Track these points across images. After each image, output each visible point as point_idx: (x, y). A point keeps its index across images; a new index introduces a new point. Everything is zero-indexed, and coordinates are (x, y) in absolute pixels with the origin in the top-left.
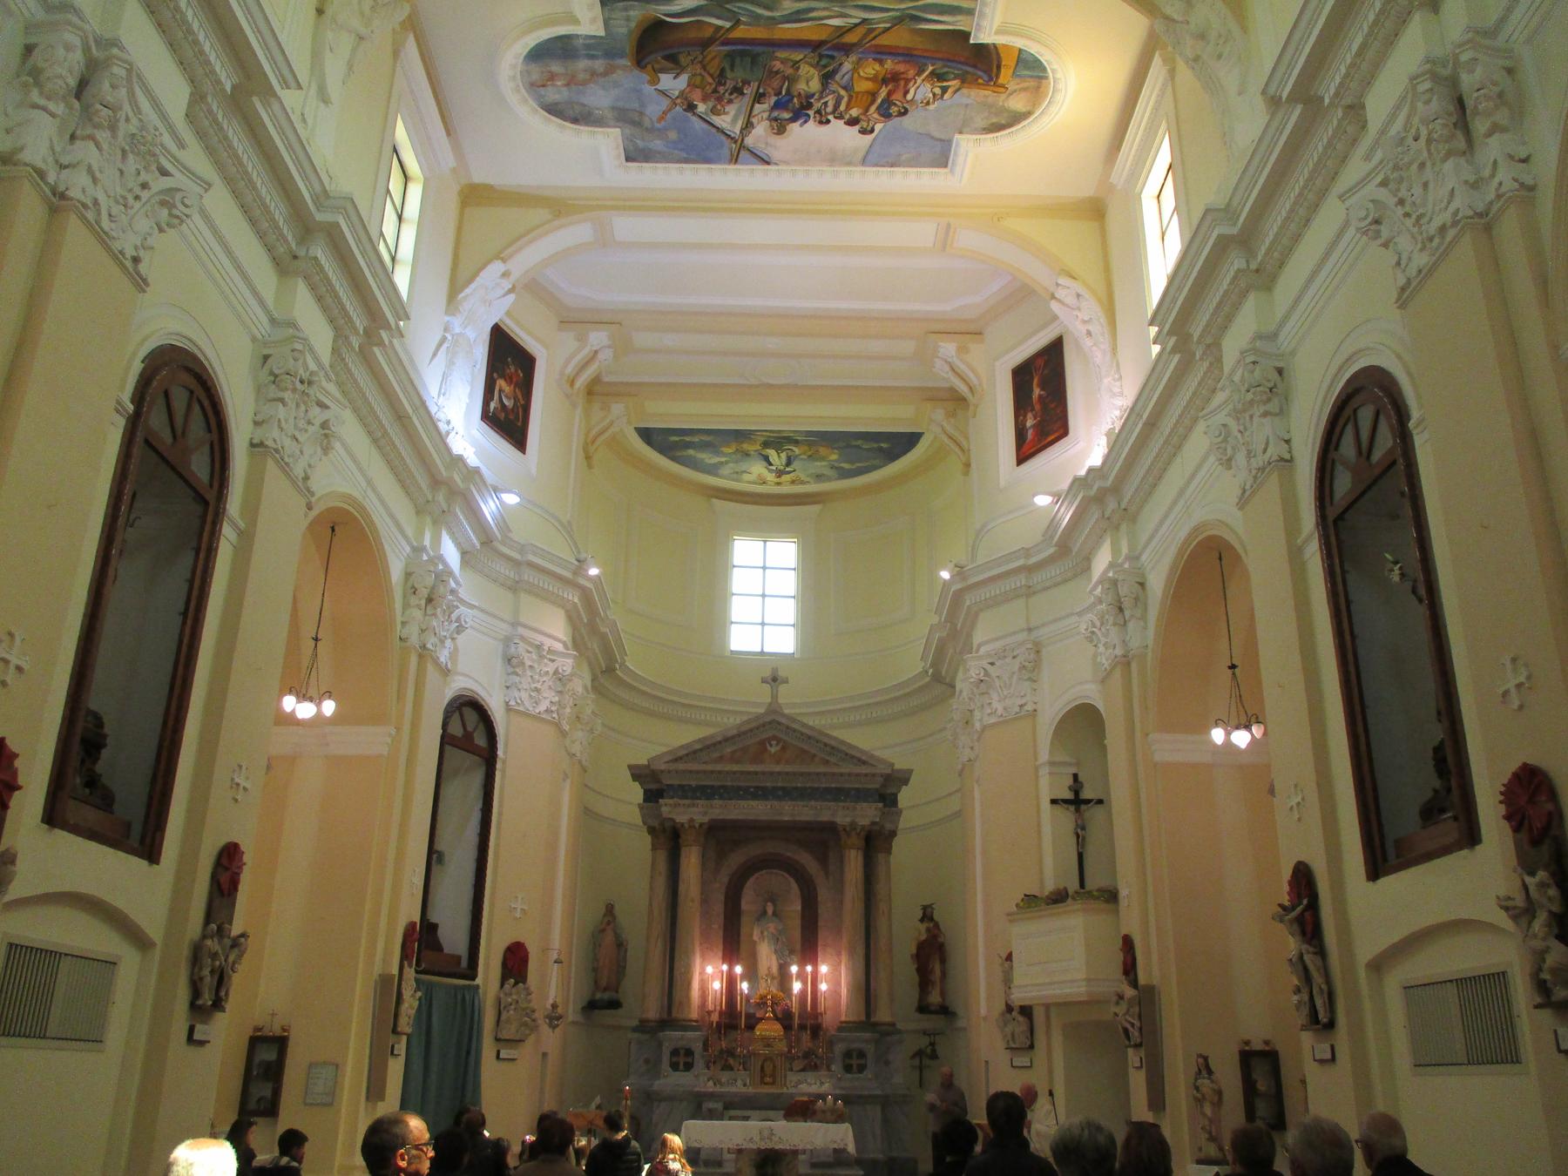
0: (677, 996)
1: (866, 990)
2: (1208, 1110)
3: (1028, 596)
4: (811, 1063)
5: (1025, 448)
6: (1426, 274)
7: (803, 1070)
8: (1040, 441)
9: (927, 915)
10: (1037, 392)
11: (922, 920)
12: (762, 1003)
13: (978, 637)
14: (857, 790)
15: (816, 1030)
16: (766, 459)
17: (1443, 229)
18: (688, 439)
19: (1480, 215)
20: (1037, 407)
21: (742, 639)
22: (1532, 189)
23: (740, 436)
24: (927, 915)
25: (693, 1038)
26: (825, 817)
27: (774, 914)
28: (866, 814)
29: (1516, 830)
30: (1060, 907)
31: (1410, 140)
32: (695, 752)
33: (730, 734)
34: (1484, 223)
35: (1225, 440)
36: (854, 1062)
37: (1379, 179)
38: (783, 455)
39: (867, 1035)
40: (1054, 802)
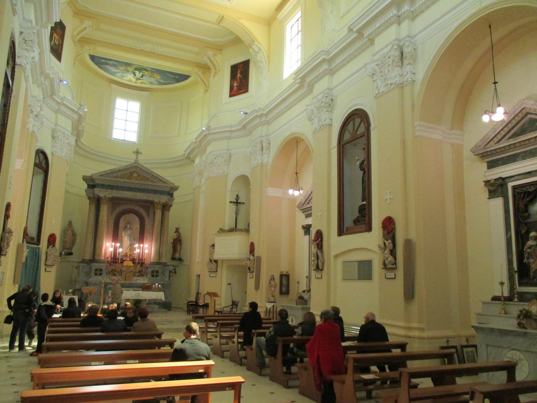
0: (97, 251)
1: (159, 253)
2: (273, 289)
3: (229, 139)
4: (141, 274)
5: (233, 92)
6: (383, 93)
7: (139, 276)
8: (238, 91)
9: (177, 231)
10: (239, 75)
11: (175, 232)
12: (126, 255)
13: (209, 149)
14: (162, 191)
15: (142, 264)
16: (134, 74)
17: (391, 84)
18: (108, 62)
19: (401, 84)
20: (238, 80)
21: (118, 134)
22: (414, 81)
23: (127, 64)
24: (177, 231)
25: (103, 266)
26: (151, 199)
27: (130, 228)
28: (164, 199)
29: (384, 230)
30: (234, 233)
31: (387, 57)
32: (108, 174)
33: (121, 169)
34: (402, 86)
35: (312, 114)
36: (155, 274)
37: (377, 63)
38: (141, 74)
39: (159, 266)
40: (231, 202)
